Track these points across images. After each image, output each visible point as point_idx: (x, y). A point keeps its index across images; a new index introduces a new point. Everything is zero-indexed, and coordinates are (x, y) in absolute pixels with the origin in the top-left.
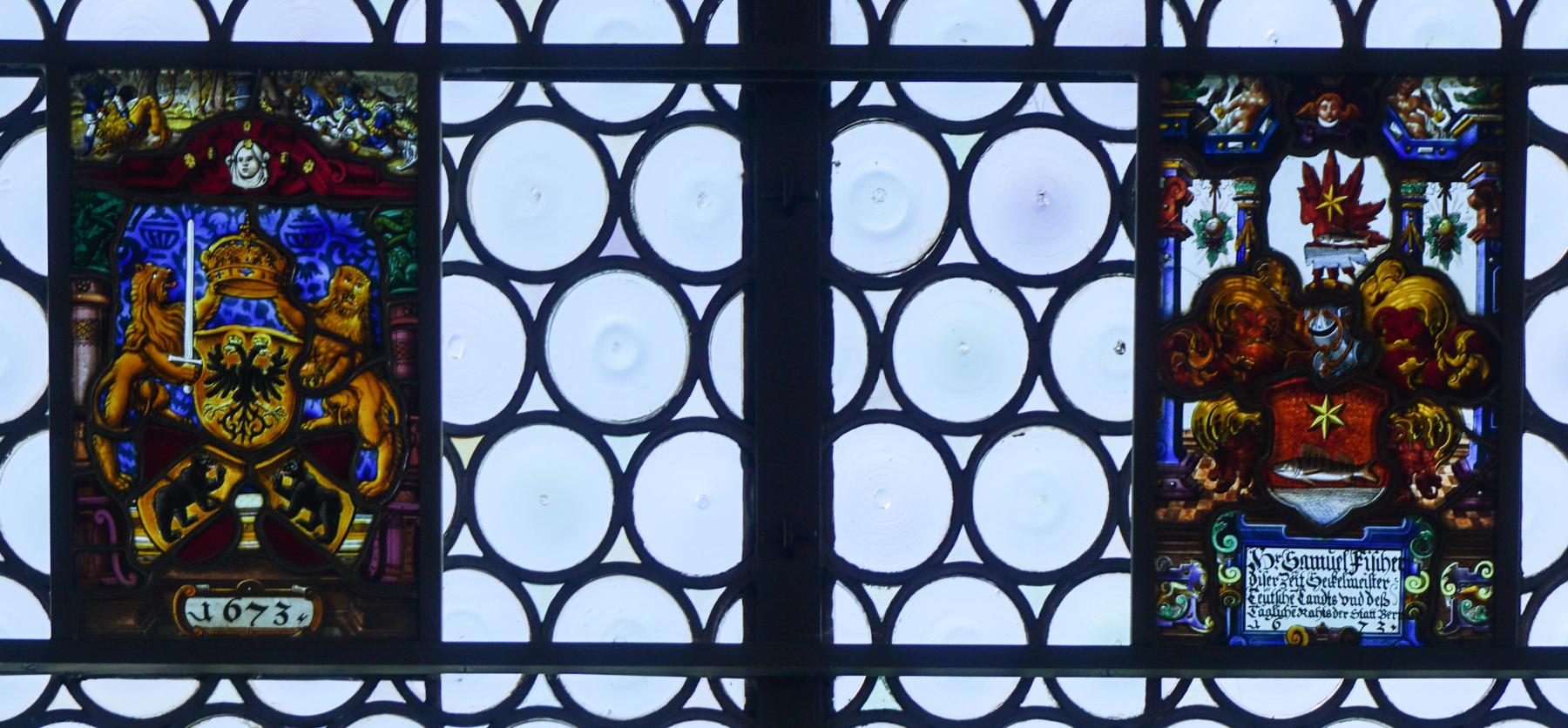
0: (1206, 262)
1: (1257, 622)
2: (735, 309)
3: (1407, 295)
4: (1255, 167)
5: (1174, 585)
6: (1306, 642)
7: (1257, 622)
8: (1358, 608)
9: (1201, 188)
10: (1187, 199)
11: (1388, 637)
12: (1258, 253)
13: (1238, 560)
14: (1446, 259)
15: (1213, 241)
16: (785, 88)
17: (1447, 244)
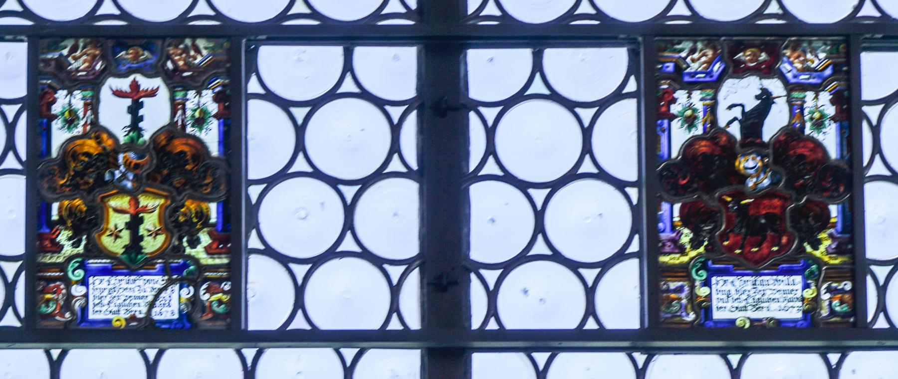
1: (717, 315)
4: (92, 83)
10: (54, 101)
12: (96, 130)
13: (84, 282)
15: (690, 122)
16: (443, 35)
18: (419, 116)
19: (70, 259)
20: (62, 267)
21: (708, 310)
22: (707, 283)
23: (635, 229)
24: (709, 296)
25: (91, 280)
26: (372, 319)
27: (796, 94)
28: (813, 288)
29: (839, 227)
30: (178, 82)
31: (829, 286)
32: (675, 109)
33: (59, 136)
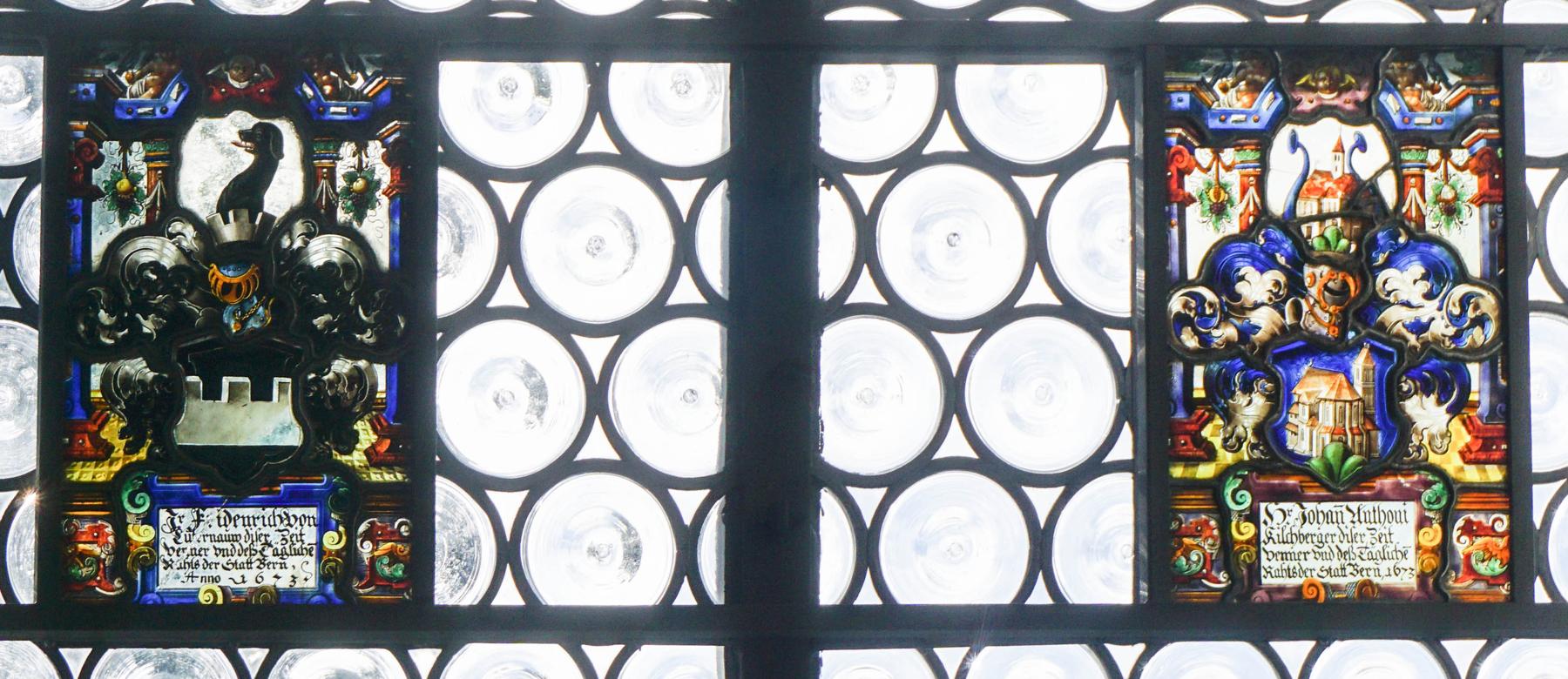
0: (117, 223)
1: (169, 580)
2: (828, 286)
3: (324, 250)
5: (1186, 540)
6: (220, 601)
7: (1274, 574)
8: (1327, 564)
9: (111, 148)
11: (301, 593)
13: (1252, 516)
14: (360, 217)
17: (362, 203)
18: (732, 195)
19: (1228, 471)
20: (1213, 488)
21: (1254, 570)
22: (150, 519)
23: (1125, 413)
24: (155, 544)
25: (164, 515)
26: (646, 587)
27: (1410, 156)
28: (1436, 526)
29: (1484, 409)
30: (321, 136)
31: (1469, 522)
32: (100, 176)
33: (104, 231)
